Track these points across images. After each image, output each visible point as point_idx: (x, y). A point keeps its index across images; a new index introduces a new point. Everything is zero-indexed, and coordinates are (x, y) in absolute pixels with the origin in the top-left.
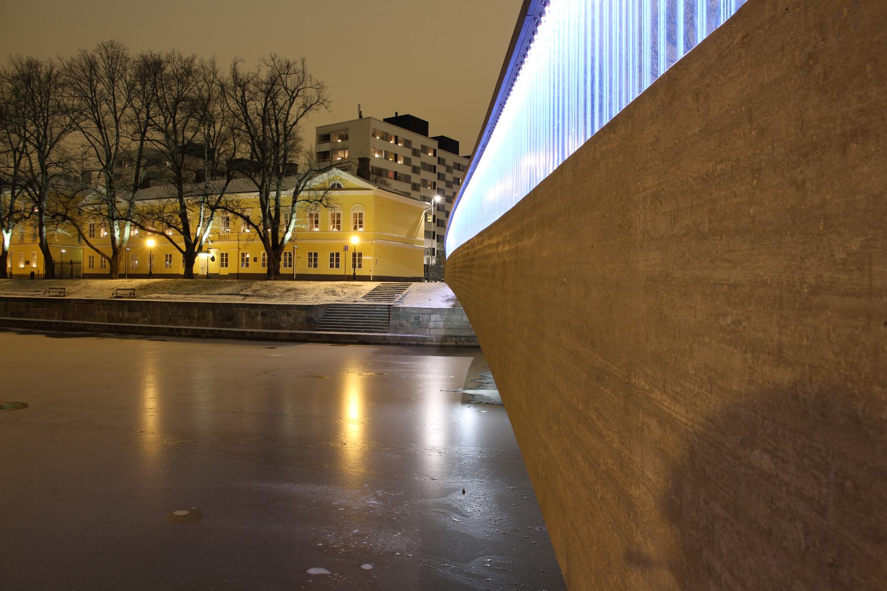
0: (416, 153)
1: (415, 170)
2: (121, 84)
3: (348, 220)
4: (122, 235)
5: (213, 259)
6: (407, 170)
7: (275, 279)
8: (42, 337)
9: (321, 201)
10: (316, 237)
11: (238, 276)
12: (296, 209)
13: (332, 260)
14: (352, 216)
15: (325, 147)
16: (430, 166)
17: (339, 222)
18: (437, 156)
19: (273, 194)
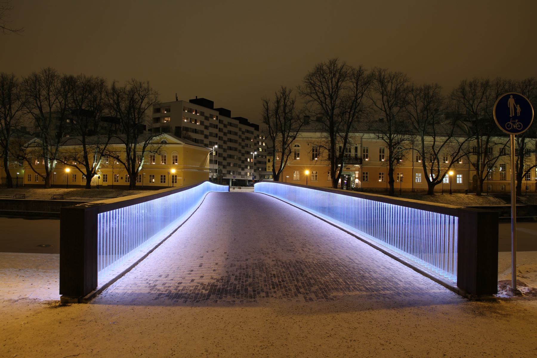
3: (170, 159)
4: (51, 165)
6: (202, 128)
7: (134, 190)
8: (22, 219)
9: (156, 152)
10: (153, 167)
11: (112, 187)
13: (162, 179)
14: (172, 157)
15: (158, 115)
16: (214, 125)
17: (165, 160)
18: (218, 119)
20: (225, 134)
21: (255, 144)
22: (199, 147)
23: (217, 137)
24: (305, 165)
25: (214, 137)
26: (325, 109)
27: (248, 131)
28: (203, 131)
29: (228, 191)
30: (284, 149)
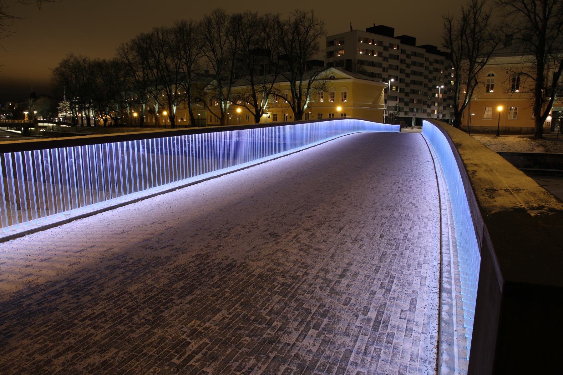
0: (386, 49)
1: (385, 59)
2: (223, 30)
3: (339, 96)
4: (225, 106)
5: (269, 117)
6: (380, 60)
10: (322, 105)
12: (309, 92)
15: (331, 49)
17: (333, 97)
19: (298, 83)
20: (408, 66)
21: (446, 77)
22: (371, 82)
23: (397, 70)
24: (497, 100)
25: (395, 69)
26: (534, 21)
27: (437, 62)
28: (382, 63)
29: (399, 132)
30: (470, 80)
